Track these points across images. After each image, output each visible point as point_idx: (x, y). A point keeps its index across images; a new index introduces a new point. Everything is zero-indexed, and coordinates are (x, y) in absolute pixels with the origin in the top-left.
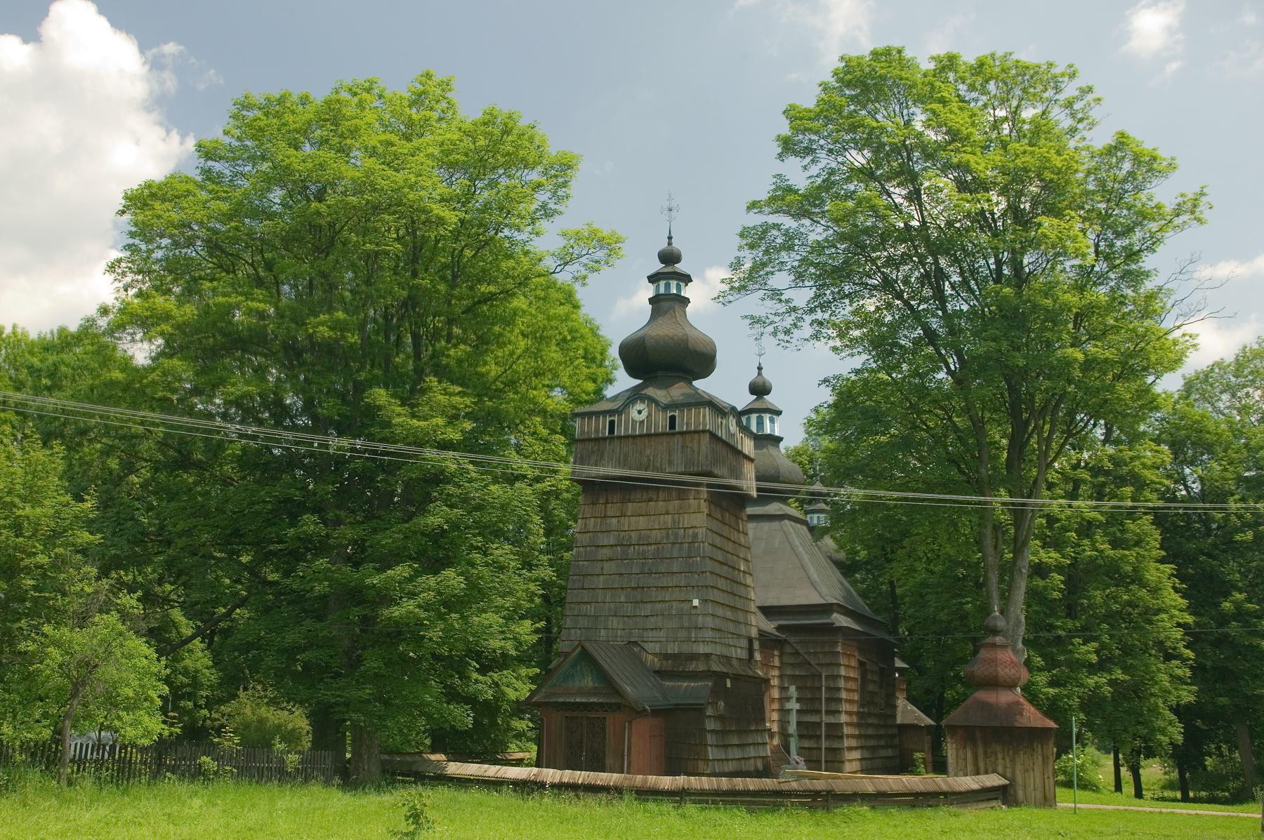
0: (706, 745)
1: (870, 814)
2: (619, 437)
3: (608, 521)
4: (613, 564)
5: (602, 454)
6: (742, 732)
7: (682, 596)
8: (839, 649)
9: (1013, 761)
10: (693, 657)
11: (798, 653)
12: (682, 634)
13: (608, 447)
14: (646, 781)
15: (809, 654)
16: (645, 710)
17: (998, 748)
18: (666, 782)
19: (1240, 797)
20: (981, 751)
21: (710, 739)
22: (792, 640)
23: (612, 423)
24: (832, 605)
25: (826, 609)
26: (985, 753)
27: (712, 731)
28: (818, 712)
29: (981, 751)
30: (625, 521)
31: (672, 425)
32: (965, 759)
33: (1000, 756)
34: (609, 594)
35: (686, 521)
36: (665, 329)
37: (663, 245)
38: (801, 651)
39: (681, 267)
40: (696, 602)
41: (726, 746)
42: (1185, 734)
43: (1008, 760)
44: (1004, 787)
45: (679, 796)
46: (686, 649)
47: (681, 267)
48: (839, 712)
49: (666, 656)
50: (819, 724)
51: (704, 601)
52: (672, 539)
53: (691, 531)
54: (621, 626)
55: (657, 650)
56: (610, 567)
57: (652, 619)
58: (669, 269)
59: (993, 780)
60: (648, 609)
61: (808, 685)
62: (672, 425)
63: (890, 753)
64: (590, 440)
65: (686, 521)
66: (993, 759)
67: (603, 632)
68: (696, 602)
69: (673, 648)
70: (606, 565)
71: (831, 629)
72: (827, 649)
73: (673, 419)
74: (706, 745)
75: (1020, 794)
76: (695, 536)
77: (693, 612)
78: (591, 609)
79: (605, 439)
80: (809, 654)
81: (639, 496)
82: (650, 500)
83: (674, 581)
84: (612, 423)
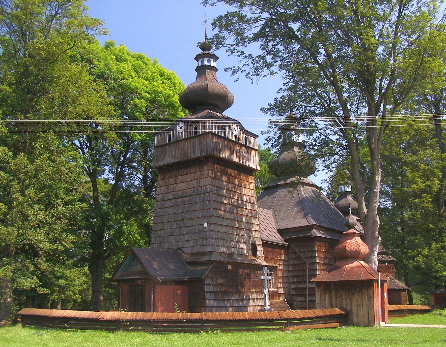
1: (221, 334)
2: (173, 143)
5: (166, 153)
7: (199, 222)
10: (204, 254)
12: (200, 243)
13: (168, 148)
16: (158, 281)
17: (343, 293)
20: (333, 296)
21: (207, 296)
22: (293, 246)
23: (170, 135)
24: (313, 225)
25: (310, 228)
26: (336, 296)
27: (210, 292)
28: (305, 282)
29: (333, 296)
32: (325, 301)
33: (344, 298)
34: (169, 224)
40: (206, 225)
43: (348, 299)
49: (193, 254)
50: (305, 289)
51: (209, 224)
54: (174, 241)
55: (189, 252)
56: (170, 211)
57: (187, 235)
60: (185, 230)
61: (301, 268)
64: (161, 146)
66: (340, 300)
67: (167, 244)
69: (196, 250)
70: (168, 209)
72: (309, 249)
75: (355, 319)
77: (205, 230)
78: (162, 232)
79: (167, 144)
81: (182, 172)
82: (187, 174)
83: (199, 214)
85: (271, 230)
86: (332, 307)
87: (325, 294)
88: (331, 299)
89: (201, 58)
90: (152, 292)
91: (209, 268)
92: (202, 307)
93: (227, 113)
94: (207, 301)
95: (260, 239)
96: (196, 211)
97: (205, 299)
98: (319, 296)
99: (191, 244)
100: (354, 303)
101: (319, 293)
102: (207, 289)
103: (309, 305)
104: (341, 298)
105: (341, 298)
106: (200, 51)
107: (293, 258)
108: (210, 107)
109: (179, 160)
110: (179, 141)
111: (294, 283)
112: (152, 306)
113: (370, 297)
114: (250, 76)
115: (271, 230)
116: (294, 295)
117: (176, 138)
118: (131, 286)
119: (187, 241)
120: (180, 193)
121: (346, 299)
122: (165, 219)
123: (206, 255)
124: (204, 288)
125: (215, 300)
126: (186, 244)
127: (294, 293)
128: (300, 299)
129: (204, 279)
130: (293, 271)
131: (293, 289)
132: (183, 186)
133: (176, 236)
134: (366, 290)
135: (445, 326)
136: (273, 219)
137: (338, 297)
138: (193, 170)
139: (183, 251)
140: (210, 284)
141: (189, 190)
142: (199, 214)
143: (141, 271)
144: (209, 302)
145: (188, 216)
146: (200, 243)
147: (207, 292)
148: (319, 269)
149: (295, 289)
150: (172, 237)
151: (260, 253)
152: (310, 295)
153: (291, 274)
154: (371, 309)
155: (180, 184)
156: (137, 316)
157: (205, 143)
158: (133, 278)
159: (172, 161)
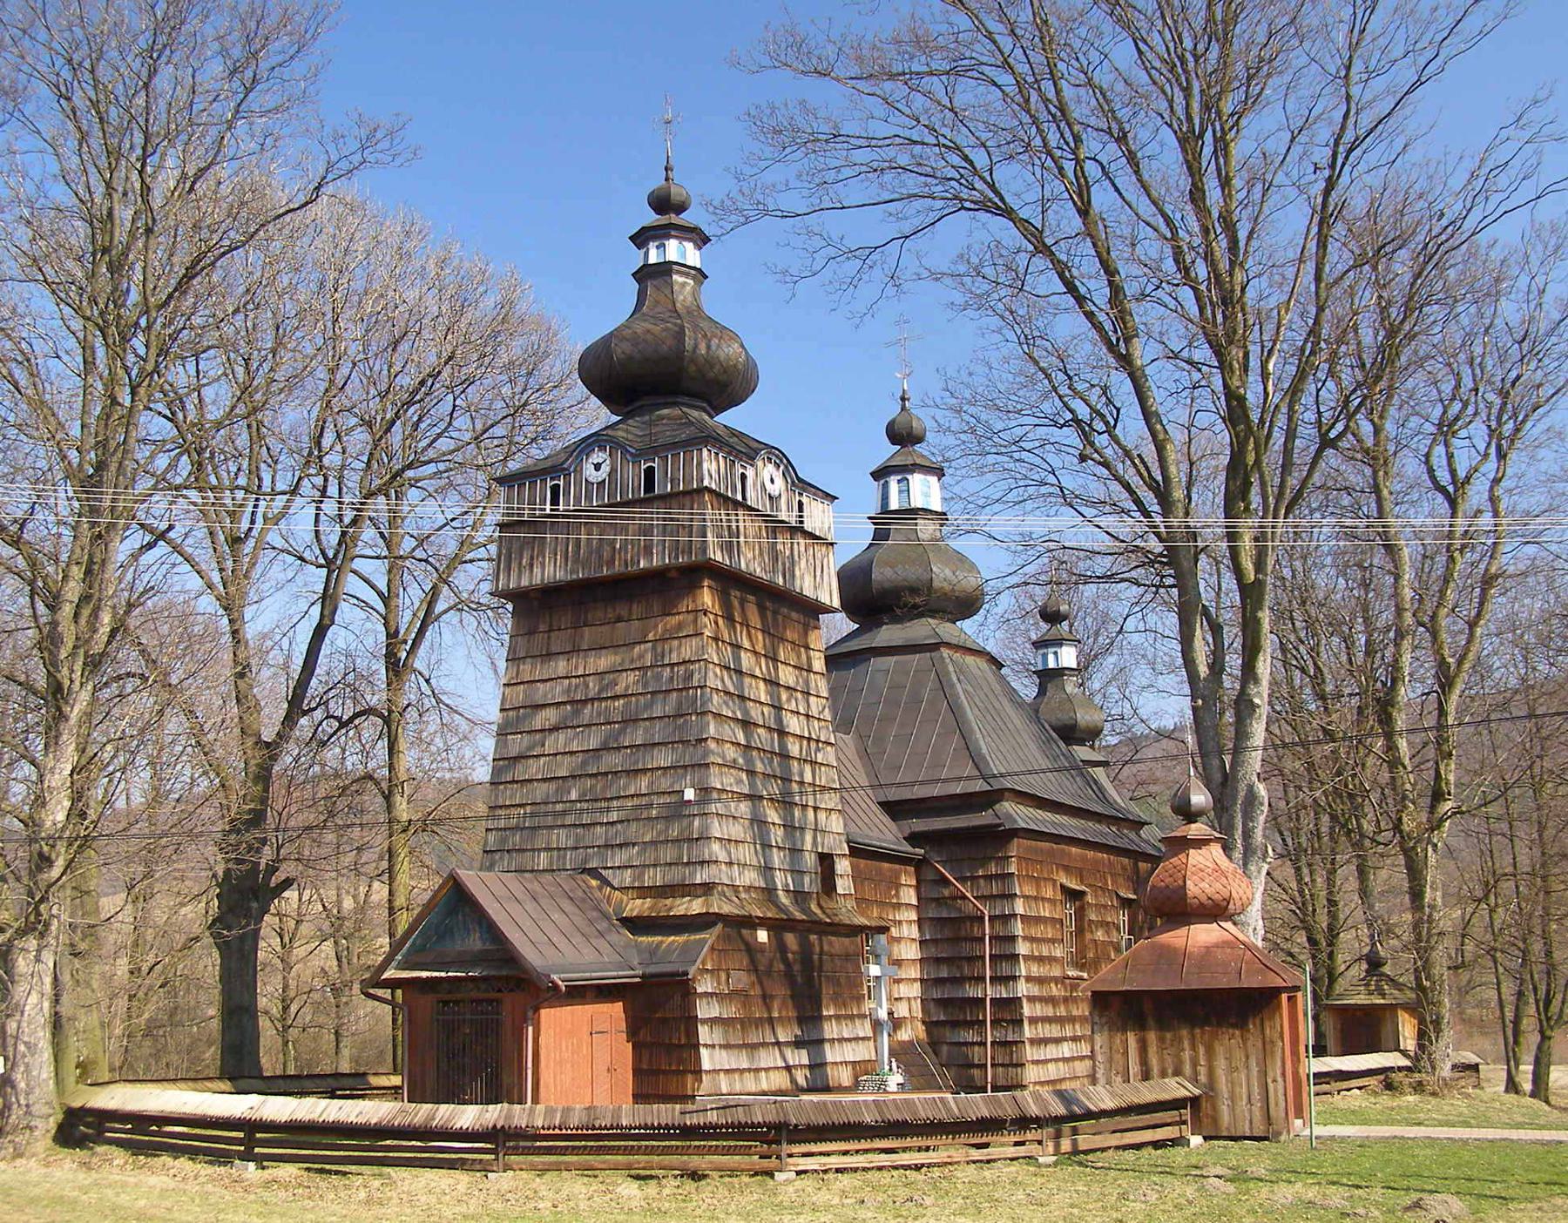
8: (1013, 869)
14: (509, 1116)
16: (556, 986)
18: (468, 1116)
19: (82, 1108)
21: (704, 1034)
22: (935, 858)
26: (1161, 1040)
27: (712, 1021)
31: (649, 485)
32: (1126, 1053)
33: (1186, 1044)
37: (657, 182)
40: (690, 794)
41: (753, 1047)
42: (14, 961)
43: (1202, 1050)
44: (1194, 1101)
45: (251, 1140)
48: (1014, 978)
54: (570, 843)
59: (1175, 1088)
62: (649, 485)
71: (1000, 836)
73: (650, 473)
81: (600, 614)
82: (619, 619)
83: (663, 758)
85: (864, 806)
86: (1146, 1076)
89: (654, 238)
91: (705, 941)
93: (730, 418)
94: (703, 1052)
95: (843, 838)
97: (697, 1046)
100: (1221, 1064)
102: (705, 1010)
103: (993, 1058)
106: (651, 218)
108: (686, 400)
115: (864, 806)
116: (937, 1022)
117: (578, 501)
118: (446, 1003)
125: (727, 1047)
127: (942, 1018)
129: (694, 980)
136: (859, 766)
139: (606, 882)
140: (711, 995)
143: (481, 952)
144: (711, 1057)
146: (668, 854)
147: (704, 1021)
148: (1025, 938)
149: (943, 1003)
151: (843, 885)
154: (1274, 1081)
156: (509, 1116)
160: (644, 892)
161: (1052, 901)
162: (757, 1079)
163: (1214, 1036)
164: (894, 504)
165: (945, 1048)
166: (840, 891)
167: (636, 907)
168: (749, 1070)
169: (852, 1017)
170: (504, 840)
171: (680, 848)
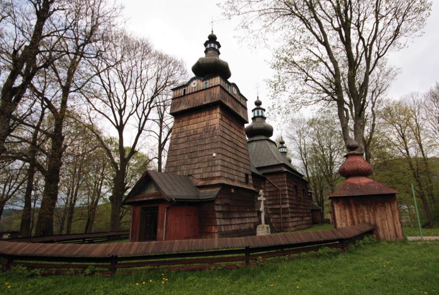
0: (216, 218)
2: (187, 95)
3: (183, 127)
4: (184, 144)
6: (240, 212)
7: (209, 153)
9: (374, 215)
11: (270, 183)
13: (182, 99)
15: (274, 182)
17: (364, 208)
20: (354, 210)
21: (217, 215)
26: (357, 211)
27: (220, 212)
30: (189, 127)
32: (346, 216)
33: (366, 212)
34: (182, 156)
35: (212, 122)
36: (212, 58)
37: (256, 99)
38: (271, 182)
39: (261, 106)
46: (211, 175)
47: (261, 106)
49: (202, 179)
52: (206, 131)
53: (213, 126)
54: (185, 169)
55: (199, 177)
56: (183, 146)
57: (197, 164)
58: (258, 107)
60: (196, 160)
61: (275, 194)
63: (308, 218)
65: (212, 122)
66: (361, 214)
68: (214, 155)
72: (281, 180)
74: (216, 218)
76: (215, 128)
79: (182, 96)
80: (274, 182)
82: (199, 117)
83: (207, 147)
84: (185, 90)
87: (345, 209)
88: (351, 214)
90: (166, 213)
92: (212, 226)
94: (218, 220)
96: (206, 144)
98: (339, 211)
99: (201, 171)
101: (339, 208)
104: (362, 212)
105: (362, 212)
107: (269, 187)
109: (192, 107)
110: (192, 93)
111: (270, 205)
112: (165, 227)
113: (395, 211)
114: (250, 47)
119: (197, 169)
120: (192, 132)
121: (368, 214)
122: (178, 152)
123: (214, 179)
124: (214, 208)
126: (196, 171)
128: (275, 216)
130: (269, 196)
131: (270, 209)
132: (195, 126)
133: (188, 166)
134: (389, 205)
135: (437, 238)
137: (359, 212)
138: (203, 114)
141: (199, 129)
142: (207, 147)
145: (199, 149)
146: (209, 169)
147: (217, 211)
149: (271, 209)
150: (183, 166)
151: (251, 181)
152: (283, 213)
153: (268, 198)
155: (192, 125)
157: (215, 93)
158: (147, 199)
159: (186, 108)
160: (202, 179)
161: (292, 188)
162: (232, 227)
163: (375, 210)
164: (256, 115)
165: (272, 219)
166: (250, 182)
167: (201, 183)
168: (230, 225)
169: (253, 212)
170: (169, 170)
171: (212, 168)
